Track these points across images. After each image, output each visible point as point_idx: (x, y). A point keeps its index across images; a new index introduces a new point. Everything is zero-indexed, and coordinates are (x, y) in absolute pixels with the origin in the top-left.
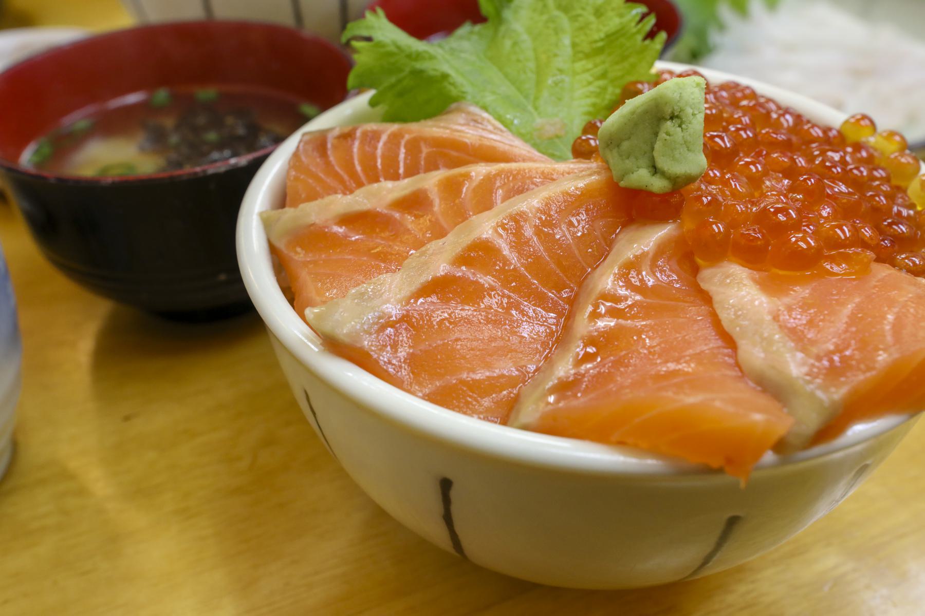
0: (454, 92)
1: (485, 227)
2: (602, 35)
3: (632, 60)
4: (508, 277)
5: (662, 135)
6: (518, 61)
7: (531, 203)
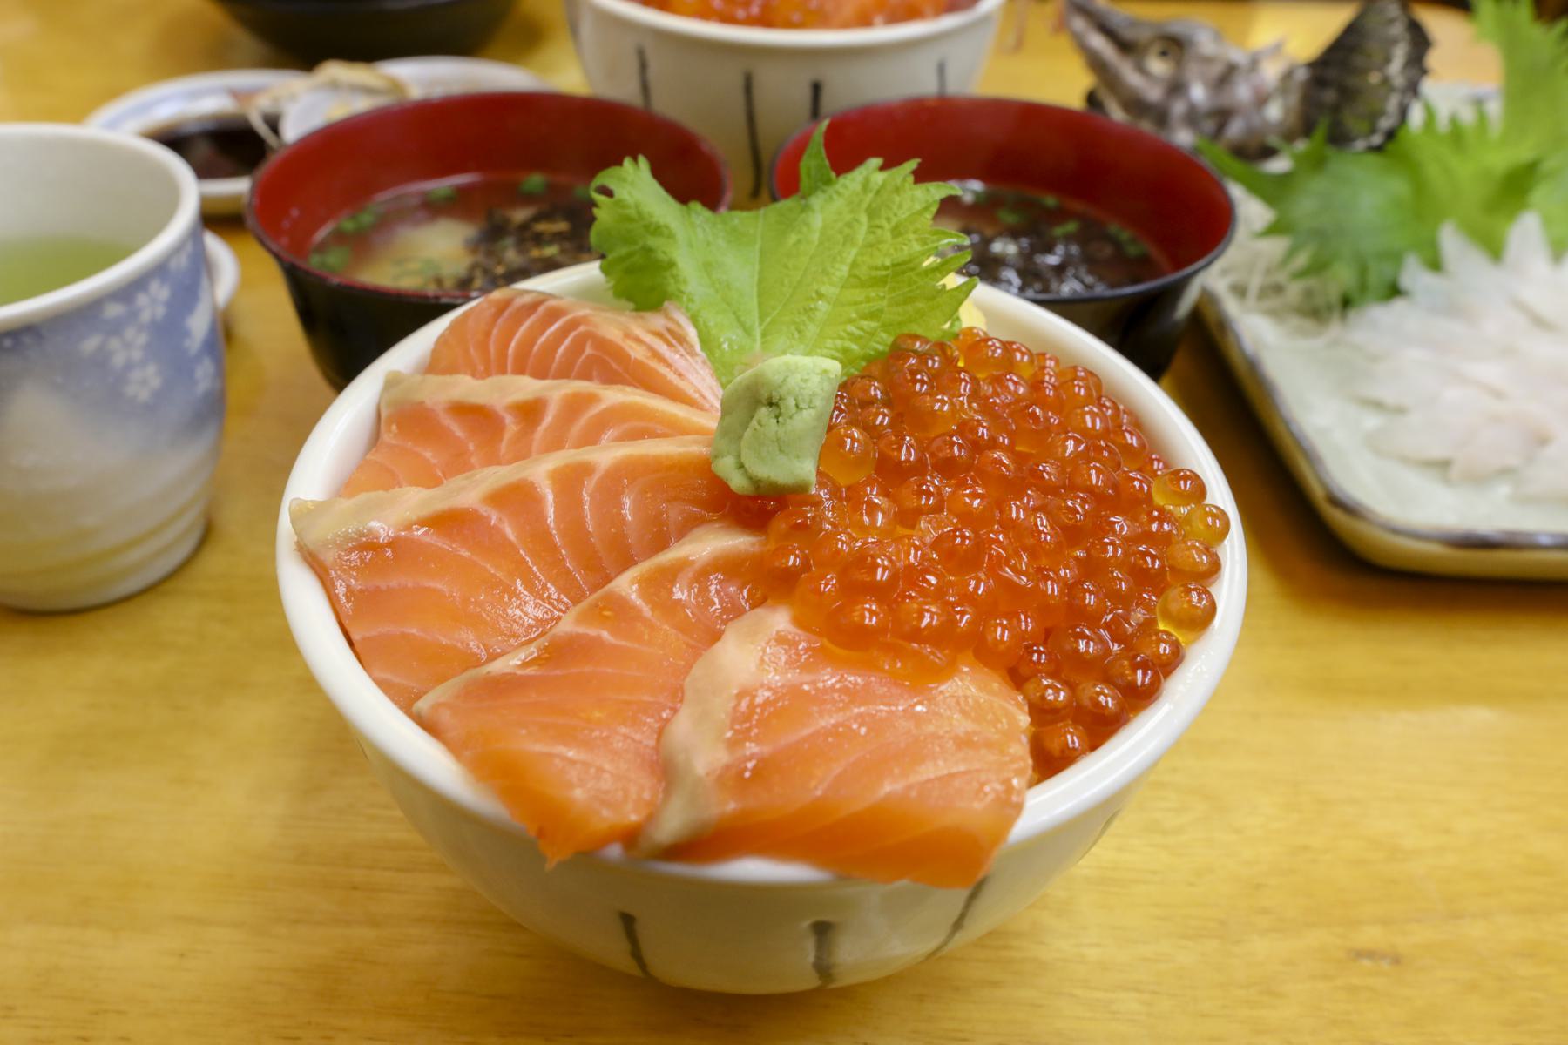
0: (672, 287)
1: (541, 471)
2: (888, 262)
3: (920, 305)
4: (540, 539)
5: (754, 423)
6: (786, 267)
7: (607, 455)
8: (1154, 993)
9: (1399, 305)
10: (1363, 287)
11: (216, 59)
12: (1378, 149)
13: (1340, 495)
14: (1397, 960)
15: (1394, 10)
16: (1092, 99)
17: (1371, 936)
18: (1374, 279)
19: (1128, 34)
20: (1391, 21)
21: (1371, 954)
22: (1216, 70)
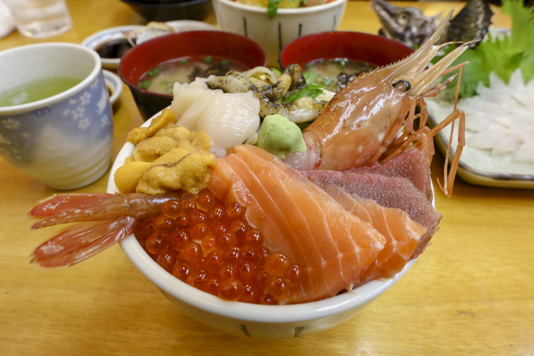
9: (476, 98)
10: (465, 92)
11: (128, 21)
12: (473, 48)
13: (462, 164)
14: (473, 315)
15: (479, 3)
16: (381, 32)
17: (464, 306)
18: (469, 90)
19: (393, 11)
20: (478, 7)
21: (464, 312)
22: (420, 23)
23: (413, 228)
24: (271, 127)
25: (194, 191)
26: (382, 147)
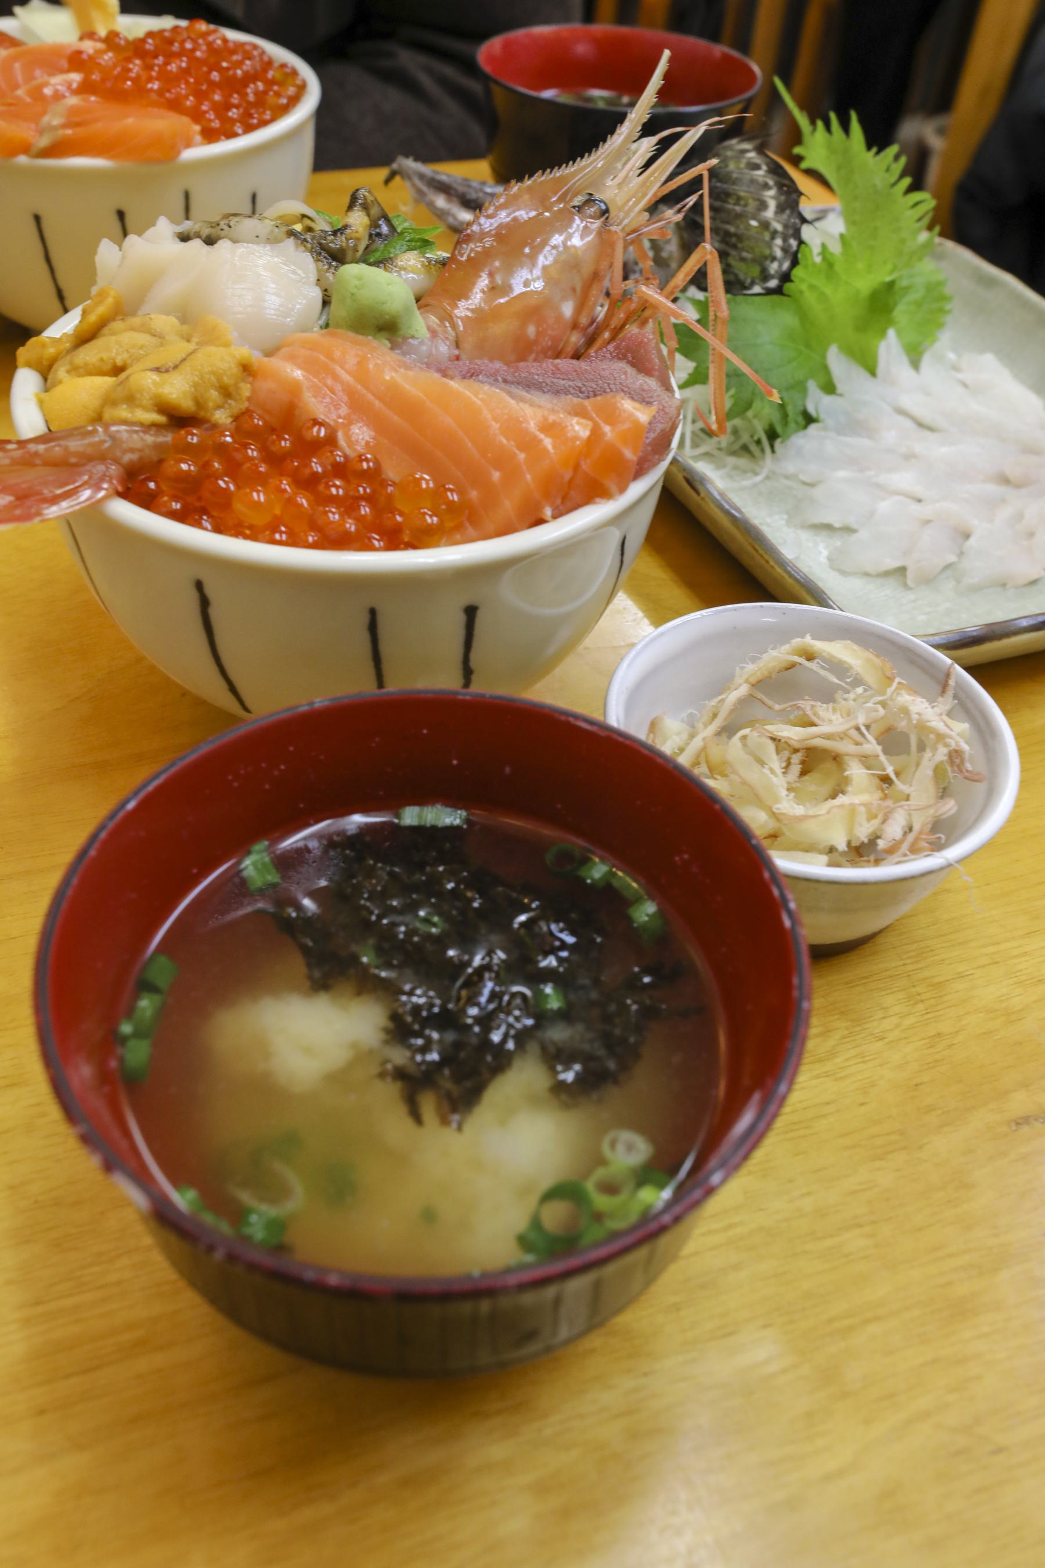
8: (874, 1222)
23: (635, 408)
24: (357, 282)
25: (222, 417)
26: (575, 332)
